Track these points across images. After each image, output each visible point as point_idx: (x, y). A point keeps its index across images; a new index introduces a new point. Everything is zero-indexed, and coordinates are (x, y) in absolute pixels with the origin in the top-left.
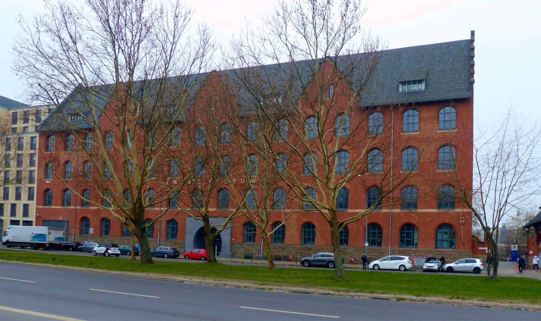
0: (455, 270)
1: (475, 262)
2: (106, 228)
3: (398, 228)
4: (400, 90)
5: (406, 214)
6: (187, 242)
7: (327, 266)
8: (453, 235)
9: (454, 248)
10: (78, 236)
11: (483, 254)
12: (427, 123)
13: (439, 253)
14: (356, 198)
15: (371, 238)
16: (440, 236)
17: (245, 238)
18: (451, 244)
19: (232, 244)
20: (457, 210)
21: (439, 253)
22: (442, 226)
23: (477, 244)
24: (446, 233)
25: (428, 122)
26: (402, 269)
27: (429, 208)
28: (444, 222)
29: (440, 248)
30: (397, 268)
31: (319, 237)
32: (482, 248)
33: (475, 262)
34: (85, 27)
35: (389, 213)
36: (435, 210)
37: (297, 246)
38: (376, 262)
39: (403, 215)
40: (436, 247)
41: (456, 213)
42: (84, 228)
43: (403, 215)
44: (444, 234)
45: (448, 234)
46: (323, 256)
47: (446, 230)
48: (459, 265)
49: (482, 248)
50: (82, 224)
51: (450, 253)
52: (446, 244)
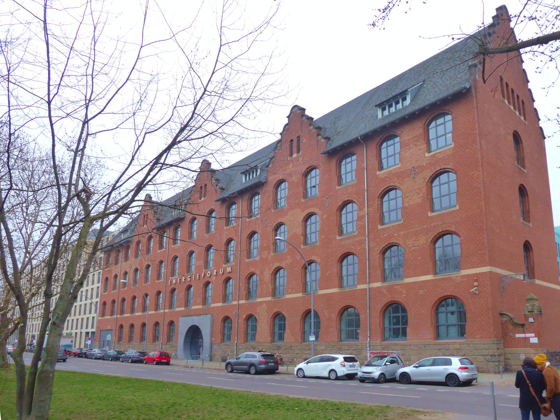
0: (413, 378)
1: (449, 363)
2: (280, 329)
3: (379, 310)
4: (380, 116)
5: (390, 289)
6: (179, 344)
7: (248, 372)
8: (462, 315)
9: (465, 338)
10: (116, 343)
11: (525, 347)
12: (410, 148)
13: (439, 347)
14: (327, 274)
15: (392, 327)
16: (442, 317)
17: (392, 333)
18: (462, 333)
19: (211, 345)
20: (464, 272)
21: (439, 347)
22: (442, 301)
23: (511, 327)
24: (452, 313)
25: (411, 145)
26: (333, 376)
27: (420, 275)
28: (445, 294)
29: (444, 339)
30: (326, 374)
31: (289, 331)
32: (523, 335)
33: (449, 363)
34: (227, 150)
35: (365, 289)
36: (429, 277)
37: (266, 344)
38: (302, 365)
39: (385, 291)
40: (438, 336)
41: (463, 277)
42: (276, 330)
43: (385, 291)
44: (449, 315)
45: (456, 314)
46: (247, 356)
47: (451, 308)
48: (422, 368)
49: (523, 335)
50: (224, 327)
51: (458, 347)
52: (453, 331)
